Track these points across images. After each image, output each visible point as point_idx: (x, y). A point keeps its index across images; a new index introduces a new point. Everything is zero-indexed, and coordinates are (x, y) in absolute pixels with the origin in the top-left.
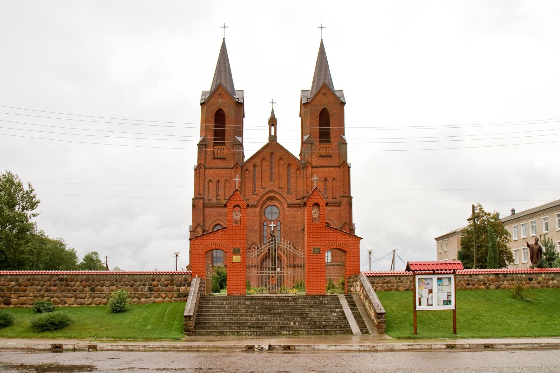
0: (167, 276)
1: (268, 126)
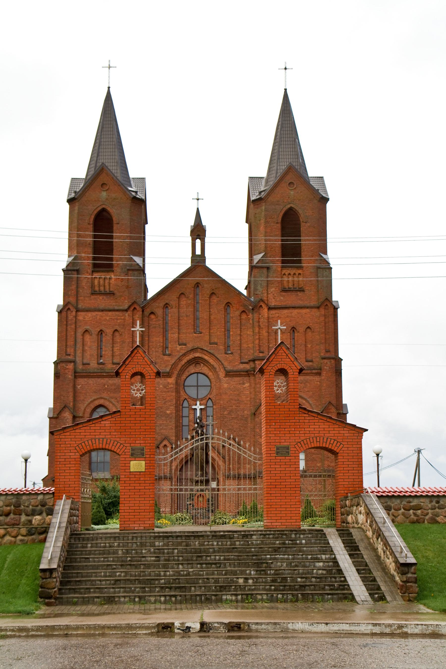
0: (9, 497)
1: (190, 238)
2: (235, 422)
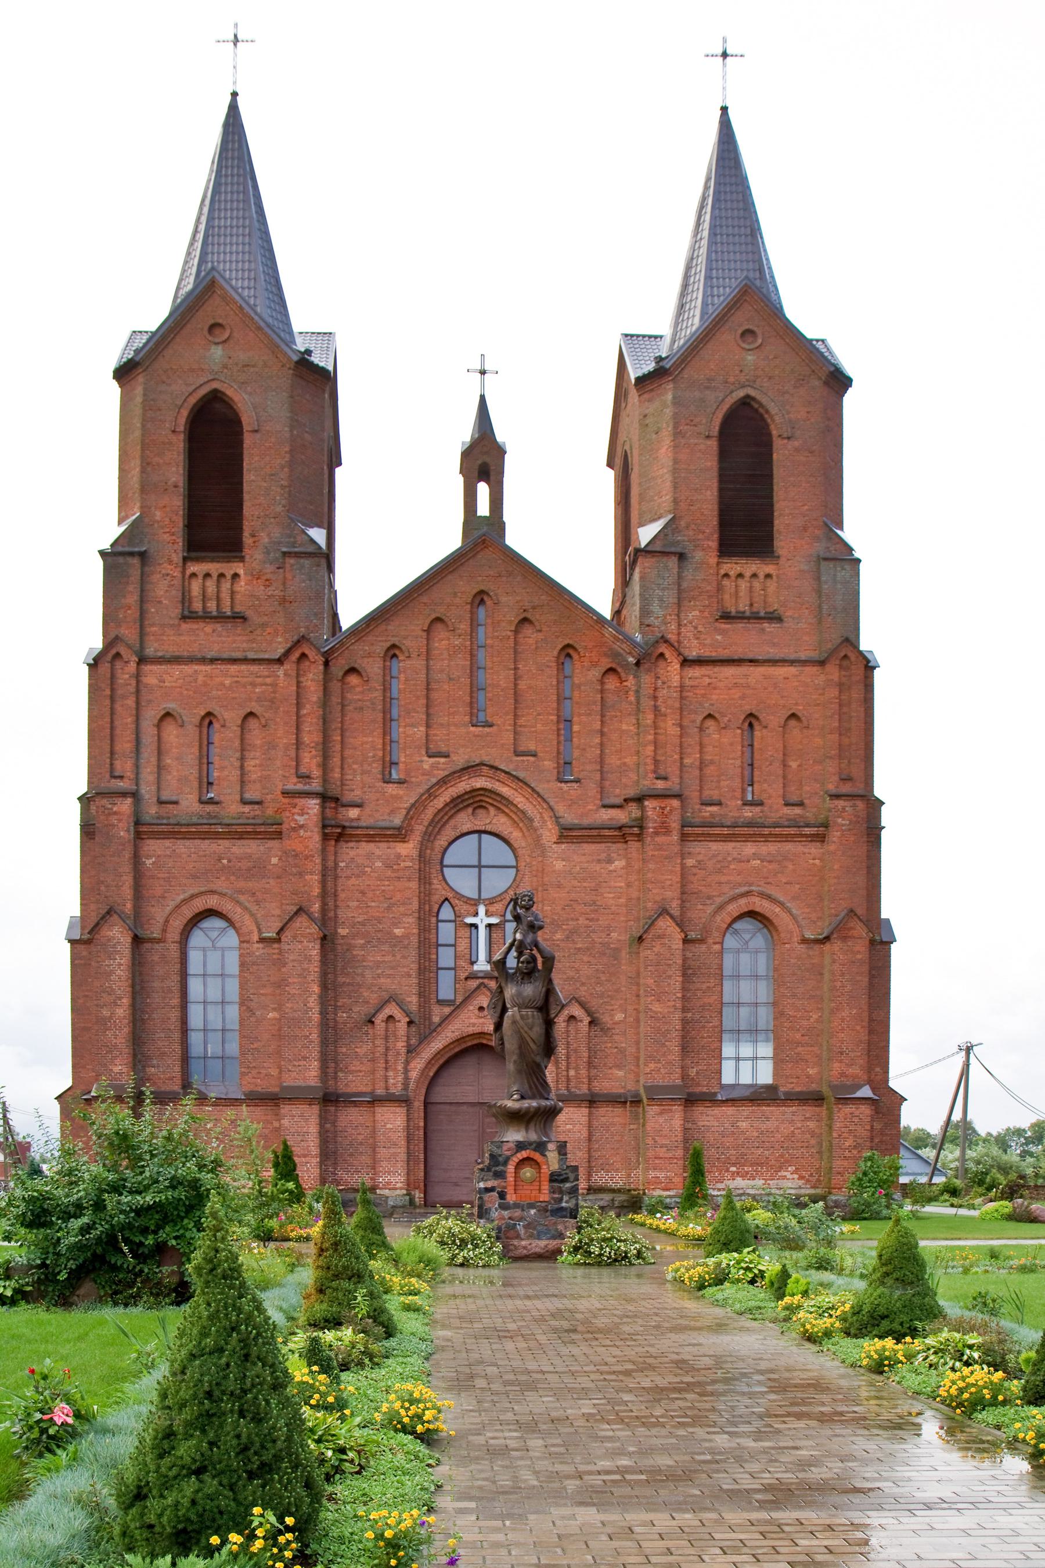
2: (585, 959)
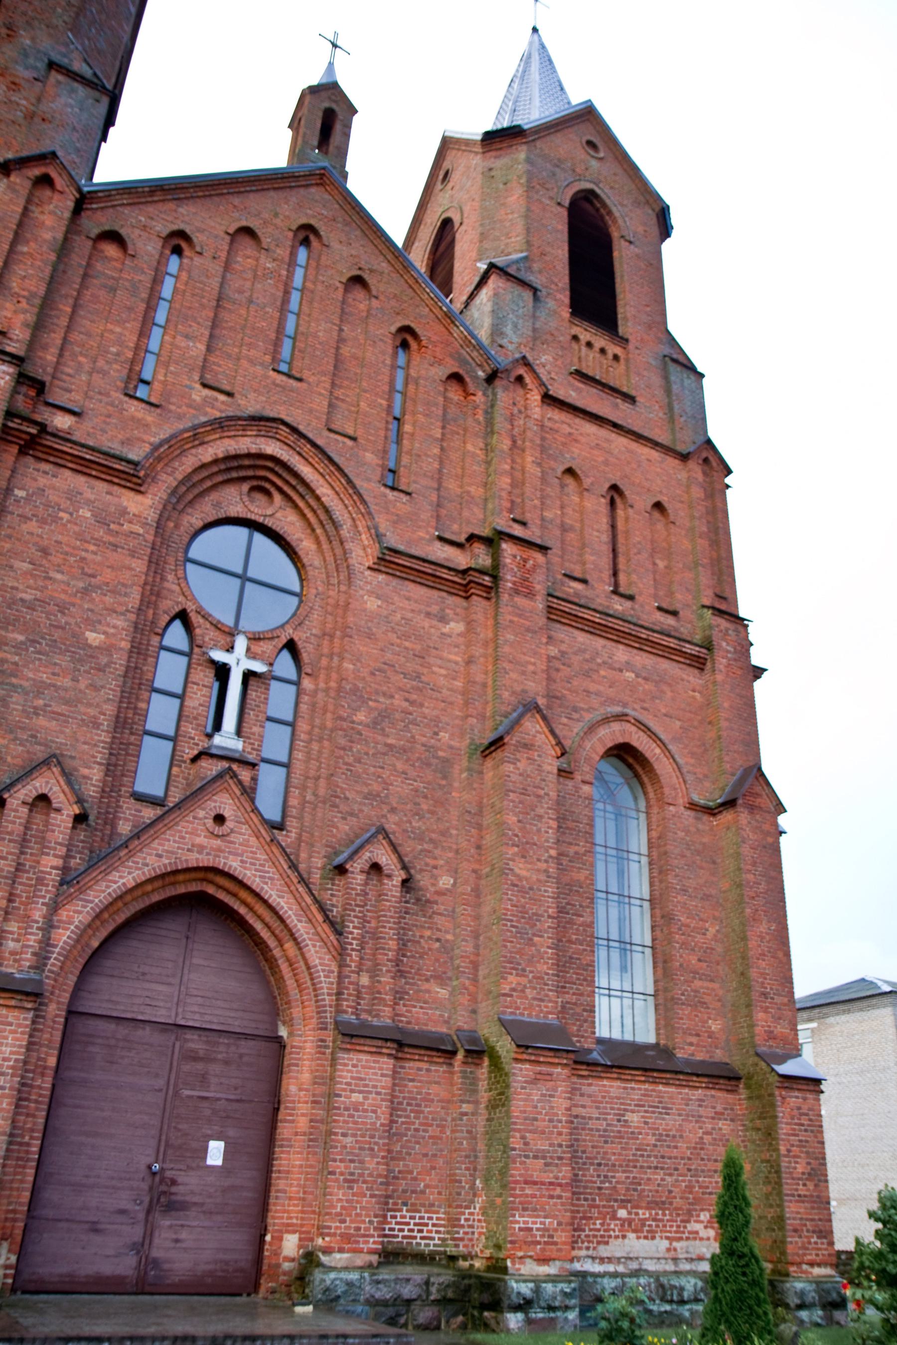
2: (400, 766)
